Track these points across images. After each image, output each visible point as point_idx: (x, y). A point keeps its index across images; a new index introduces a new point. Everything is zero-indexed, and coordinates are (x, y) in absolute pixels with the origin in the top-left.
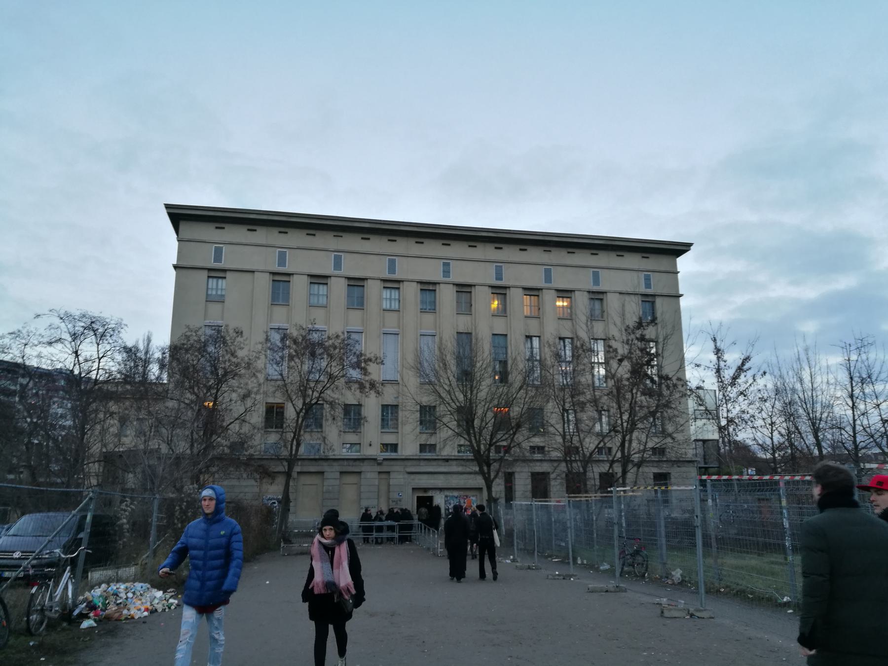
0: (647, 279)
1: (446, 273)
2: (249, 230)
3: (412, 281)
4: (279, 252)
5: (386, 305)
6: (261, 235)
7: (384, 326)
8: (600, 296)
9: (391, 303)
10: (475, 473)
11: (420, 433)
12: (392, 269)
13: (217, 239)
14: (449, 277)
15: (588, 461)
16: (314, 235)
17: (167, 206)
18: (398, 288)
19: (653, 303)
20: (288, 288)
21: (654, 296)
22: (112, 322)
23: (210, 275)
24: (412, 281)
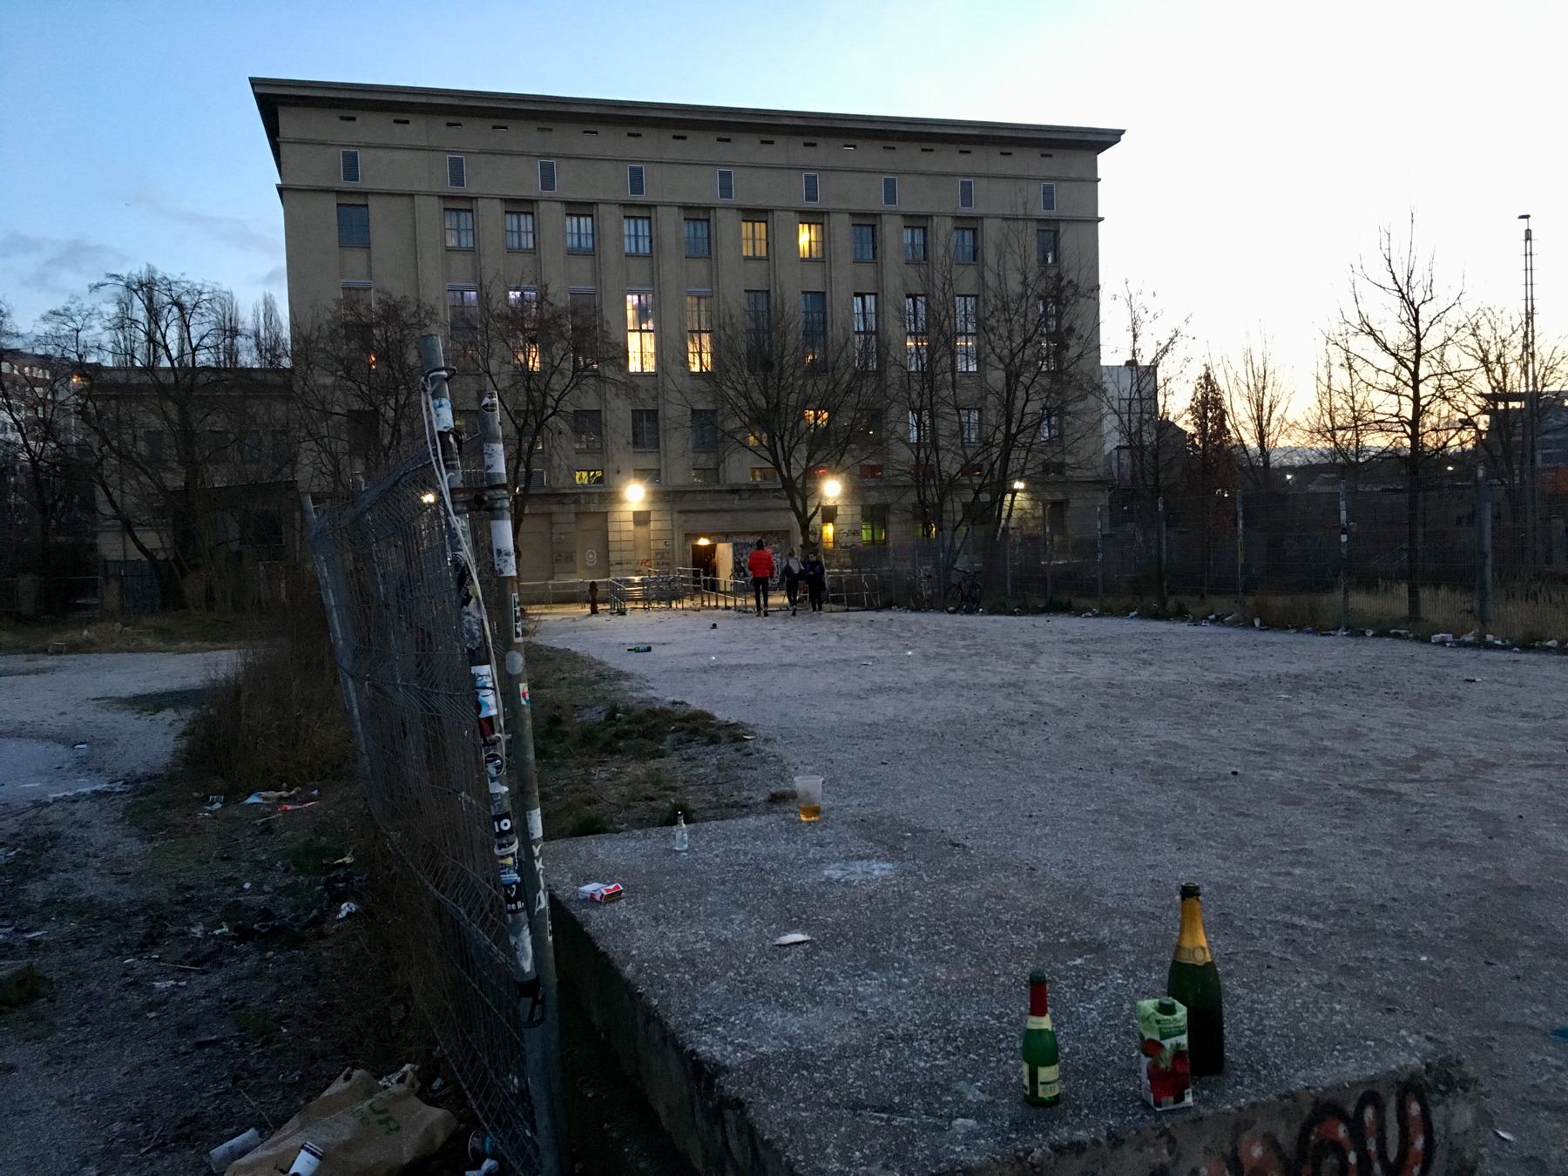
0: (890, 187)
1: (726, 190)
4: (450, 159)
5: (629, 246)
6: (418, 130)
8: (973, 224)
9: (520, 238)
10: (787, 509)
15: (951, 486)
17: (255, 82)
18: (471, 211)
19: (1056, 233)
21: (1057, 221)
22: (205, 290)
23: (342, 202)
24: (670, 205)
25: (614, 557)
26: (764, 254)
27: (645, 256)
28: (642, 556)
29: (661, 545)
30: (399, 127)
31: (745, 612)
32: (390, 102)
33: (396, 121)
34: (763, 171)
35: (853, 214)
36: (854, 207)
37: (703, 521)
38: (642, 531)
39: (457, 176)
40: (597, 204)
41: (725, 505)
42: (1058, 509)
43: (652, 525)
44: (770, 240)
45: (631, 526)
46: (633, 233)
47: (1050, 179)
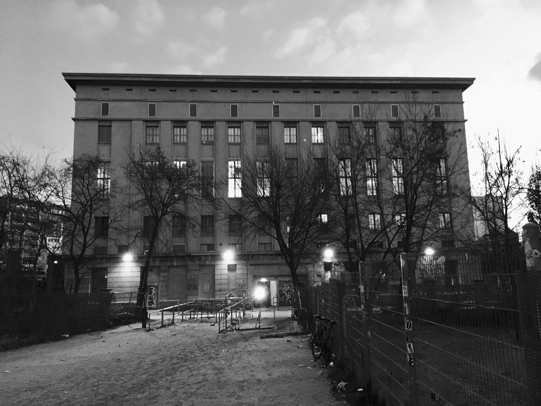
2: (171, 91)
3: (250, 121)
5: (231, 140)
7: (202, 156)
11: (173, 236)
12: (318, 114)
13: (232, 99)
14: (279, 117)
16: (175, 91)
17: (64, 75)
20: (110, 131)
23: (147, 125)
24: (250, 121)
25: (217, 287)
26: (295, 142)
27: (238, 144)
28: (232, 287)
29: (241, 282)
30: (127, 92)
31: (201, 322)
32: (118, 81)
33: (127, 90)
34: (339, 104)
35: (338, 122)
36: (338, 119)
37: (262, 269)
38: (232, 274)
39: (152, 111)
40: (243, 121)
41: (274, 262)
42: (451, 265)
43: (238, 271)
44: (298, 136)
45: (226, 272)
46: (206, 134)
47: (395, 103)
